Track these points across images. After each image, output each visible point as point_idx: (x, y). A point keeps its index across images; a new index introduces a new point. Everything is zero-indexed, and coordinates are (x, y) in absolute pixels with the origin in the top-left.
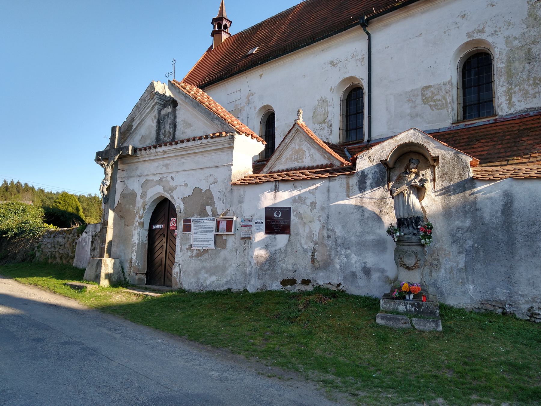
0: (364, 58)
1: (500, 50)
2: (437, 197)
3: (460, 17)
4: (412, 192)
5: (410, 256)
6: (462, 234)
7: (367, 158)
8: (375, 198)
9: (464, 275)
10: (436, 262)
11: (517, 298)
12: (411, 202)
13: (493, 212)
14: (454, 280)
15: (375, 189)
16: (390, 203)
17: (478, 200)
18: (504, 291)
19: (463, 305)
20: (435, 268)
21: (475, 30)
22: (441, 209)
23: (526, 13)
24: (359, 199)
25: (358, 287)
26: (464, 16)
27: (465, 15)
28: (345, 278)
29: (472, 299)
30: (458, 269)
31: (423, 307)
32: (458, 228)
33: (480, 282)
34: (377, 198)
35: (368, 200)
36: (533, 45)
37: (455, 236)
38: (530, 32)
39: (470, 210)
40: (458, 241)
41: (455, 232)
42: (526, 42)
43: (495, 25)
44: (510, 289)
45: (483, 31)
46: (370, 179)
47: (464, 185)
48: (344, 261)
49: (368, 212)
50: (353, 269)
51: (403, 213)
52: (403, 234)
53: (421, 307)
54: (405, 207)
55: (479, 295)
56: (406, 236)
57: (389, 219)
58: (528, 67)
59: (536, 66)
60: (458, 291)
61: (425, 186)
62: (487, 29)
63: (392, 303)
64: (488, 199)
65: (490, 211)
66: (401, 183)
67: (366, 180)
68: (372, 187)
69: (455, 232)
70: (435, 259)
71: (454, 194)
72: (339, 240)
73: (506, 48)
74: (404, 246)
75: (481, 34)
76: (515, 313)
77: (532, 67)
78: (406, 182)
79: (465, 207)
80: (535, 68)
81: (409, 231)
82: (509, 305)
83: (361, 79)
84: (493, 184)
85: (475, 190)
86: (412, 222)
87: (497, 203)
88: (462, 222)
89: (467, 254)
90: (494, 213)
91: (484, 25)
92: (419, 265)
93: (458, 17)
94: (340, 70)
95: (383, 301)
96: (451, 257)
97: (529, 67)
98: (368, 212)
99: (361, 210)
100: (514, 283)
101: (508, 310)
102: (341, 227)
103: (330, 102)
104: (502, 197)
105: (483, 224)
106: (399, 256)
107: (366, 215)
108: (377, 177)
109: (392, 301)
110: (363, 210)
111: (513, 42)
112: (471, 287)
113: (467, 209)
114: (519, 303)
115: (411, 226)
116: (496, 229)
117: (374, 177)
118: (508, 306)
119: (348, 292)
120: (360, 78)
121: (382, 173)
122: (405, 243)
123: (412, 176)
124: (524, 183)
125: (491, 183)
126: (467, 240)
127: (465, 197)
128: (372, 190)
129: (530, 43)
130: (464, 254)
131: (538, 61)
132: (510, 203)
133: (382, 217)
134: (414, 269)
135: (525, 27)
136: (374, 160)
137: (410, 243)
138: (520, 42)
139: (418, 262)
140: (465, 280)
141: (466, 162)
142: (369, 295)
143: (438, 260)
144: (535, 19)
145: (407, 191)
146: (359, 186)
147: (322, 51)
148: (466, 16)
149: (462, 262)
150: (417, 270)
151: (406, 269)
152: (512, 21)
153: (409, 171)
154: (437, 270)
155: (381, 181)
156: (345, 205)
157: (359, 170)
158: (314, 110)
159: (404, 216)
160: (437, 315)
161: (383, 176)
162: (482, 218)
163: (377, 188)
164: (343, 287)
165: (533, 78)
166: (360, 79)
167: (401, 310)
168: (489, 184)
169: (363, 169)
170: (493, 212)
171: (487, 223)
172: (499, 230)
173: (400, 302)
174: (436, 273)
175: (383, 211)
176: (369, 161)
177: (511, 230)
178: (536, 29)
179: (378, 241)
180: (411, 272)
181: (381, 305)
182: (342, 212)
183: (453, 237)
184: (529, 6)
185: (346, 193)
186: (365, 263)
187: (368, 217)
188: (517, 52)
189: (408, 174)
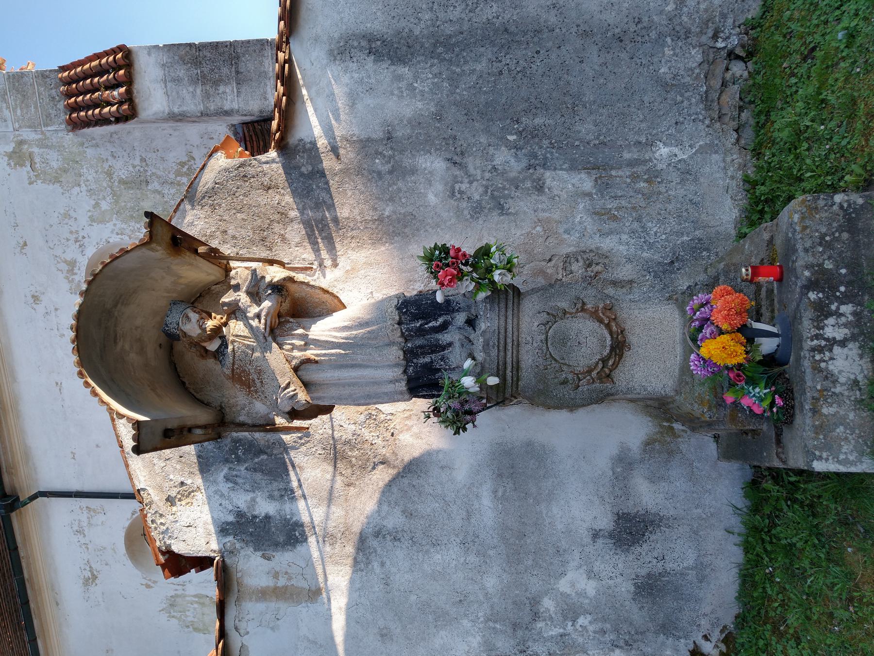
0: (87, 507)
1: (115, 232)
2: (341, 261)
3: (35, 306)
4: (300, 331)
5: (563, 340)
6: (471, 183)
7: (174, 509)
8: (329, 484)
9: (620, 173)
10: (577, 267)
11: (690, 15)
12: (339, 337)
13: (399, 88)
14: (643, 204)
15: (295, 484)
16: (353, 427)
17: (357, 132)
18: (668, 52)
19: (732, 178)
20: (599, 268)
21: (67, 278)
22: (383, 248)
23: (51, 187)
24: (328, 548)
25: (702, 571)
26: (36, 299)
27: (33, 296)
28: (668, 628)
29: (711, 148)
30: (601, 192)
31: (829, 265)
32: (453, 194)
33: (643, 125)
34: (329, 476)
35: (337, 512)
36: (114, 176)
37: (479, 202)
38: (88, 181)
39: (390, 157)
40: (495, 193)
41: (464, 204)
42: (106, 188)
43: (63, 241)
44: (661, 35)
45: (72, 264)
46: (253, 500)
47: (302, 175)
48: (591, 628)
49: (383, 514)
50: (626, 588)
51: (383, 367)
52: (468, 364)
53: (822, 271)
54: (359, 358)
55: (689, 127)
56: (480, 356)
57: (415, 429)
58: (155, 185)
59: (154, 171)
60: (682, 192)
61: (275, 280)
62: (69, 257)
63: (825, 411)
64: (354, 104)
65: (395, 98)
66: (260, 372)
67: (255, 517)
68: (288, 494)
69: (464, 204)
70: (564, 269)
71: (331, 207)
72: (499, 644)
73: (112, 223)
74: (523, 365)
75: (77, 267)
76: (741, 21)
77: (157, 177)
78: (257, 354)
79: (379, 173)
80: (159, 173)
81: (457, 345)
82: (715, 37)
83: (133, 514)
84: (304, 92)
85: (322, 143)
86: (421, 332)
87: (369, 77)
88: (430, 183)
89: (544, 166)
90: (403, 84)
91: (60, 261)
92: (601, 306)
93: (35, 309)
94: (107, 564)
95: (820, 458)
96: (556, 216)
97: (156, 184)
98: (383, 514)
99: (374, 543)
100: (639, 26)
101: (735, 41)
102: (443, 633)
103: (176, 590)
104: (351, 65)
105: (438, 116)
106: (565, 382)
107: (394, 520)
108: (248, 474)
109: (815, 411)
110: (377, 534)
111: (103, 209)
112: (664, 150)
113: (388, 167)
114: (706, 10)
115: (439, 336)
116: (454, 81)
117: (247, 487)
118: (720, 40)
119: (728, 620)
120: (132, 517)
121: (236, 454)
122: (509, 360)
123: (236, 328)
124: (310, 7)
125: (303, 96)
126: (494, 168)
127: (345, 172)
128: (298, 493)
129: (110, 181)
130: (542, 175)
131: (146, 168)
132: (369, 41)
133: (407, 458)
134: (617, 325)
135: (77, 189)
136: (182, 484)
137: (509, 341)
138: (104, 198)
139: (589, 306)
140: (639, 169)
141: (226, 170)
142: (735, 523)
143: (568, 259)
144: (65, 171)
145: (294, 347)
146: (276, 545)
147: (57, 604)
148: (36, 294)
149: (573, 181)
150: (623, 315)
151: (621, 357)
152: (62, 211)
153: (211, 338)
154: (607, 261)
155: (265, 457)
156: (351, 609)
157: (214, 546)
158: (191, 629)
159: (397, 365)
160: (860, 201)
161: (247, 451)
162: (416, 122)
163: (292, 473)
164: (706, 638)
165: (176, 177)
166: (134, 516)
167: (856, 370)
168: (304, 102)
169: (212, 528)
170: (399, 88)
171: (436, 105)
172: (458, 70)
173: (817, 369)
174: (618, 265)
175: (384, 451)
176: (183, 503)
177: (460, 38)
178: (85, 170)
179: (500, 475)
180: (632, 339)
181: (842, 469)
182: (381, 623)
183: (482, 208)
184: (39, 182)
185: (299, 603)
186: (596, 535)
187: (403, 512)
188: (123, 204)
189: (224, 344)
